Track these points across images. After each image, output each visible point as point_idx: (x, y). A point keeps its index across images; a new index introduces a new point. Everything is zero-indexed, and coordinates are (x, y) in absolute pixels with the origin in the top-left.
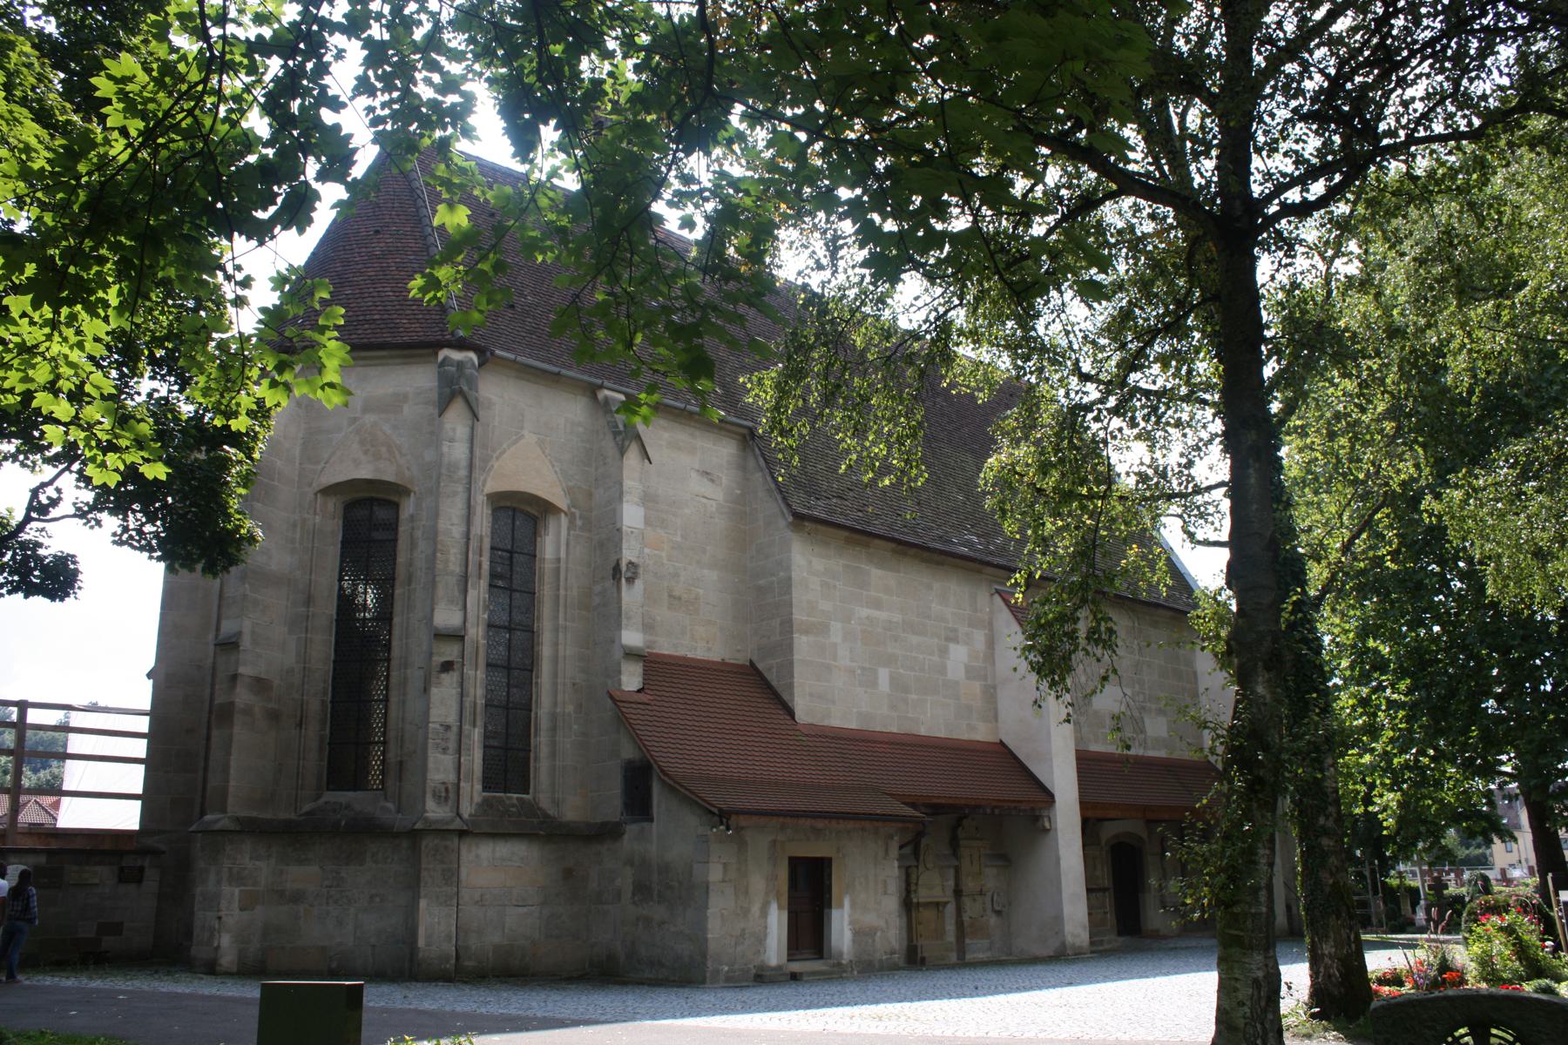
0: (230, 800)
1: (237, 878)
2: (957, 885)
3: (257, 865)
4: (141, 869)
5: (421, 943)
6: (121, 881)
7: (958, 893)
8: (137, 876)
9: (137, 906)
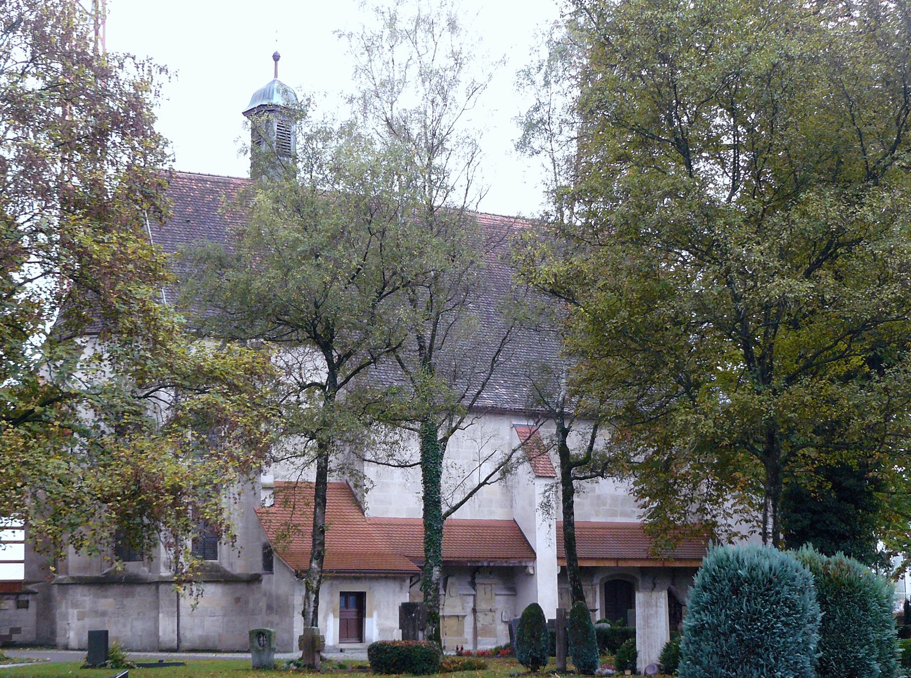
0: (70, 568)
1: (75, 605)
2: (475, 605)
3: (84, 597)
4: (28, 601)
5: (161, 634)
6: (18, 607)
7: (474, 611)
8: (25, 605)
9: (27, 620)
